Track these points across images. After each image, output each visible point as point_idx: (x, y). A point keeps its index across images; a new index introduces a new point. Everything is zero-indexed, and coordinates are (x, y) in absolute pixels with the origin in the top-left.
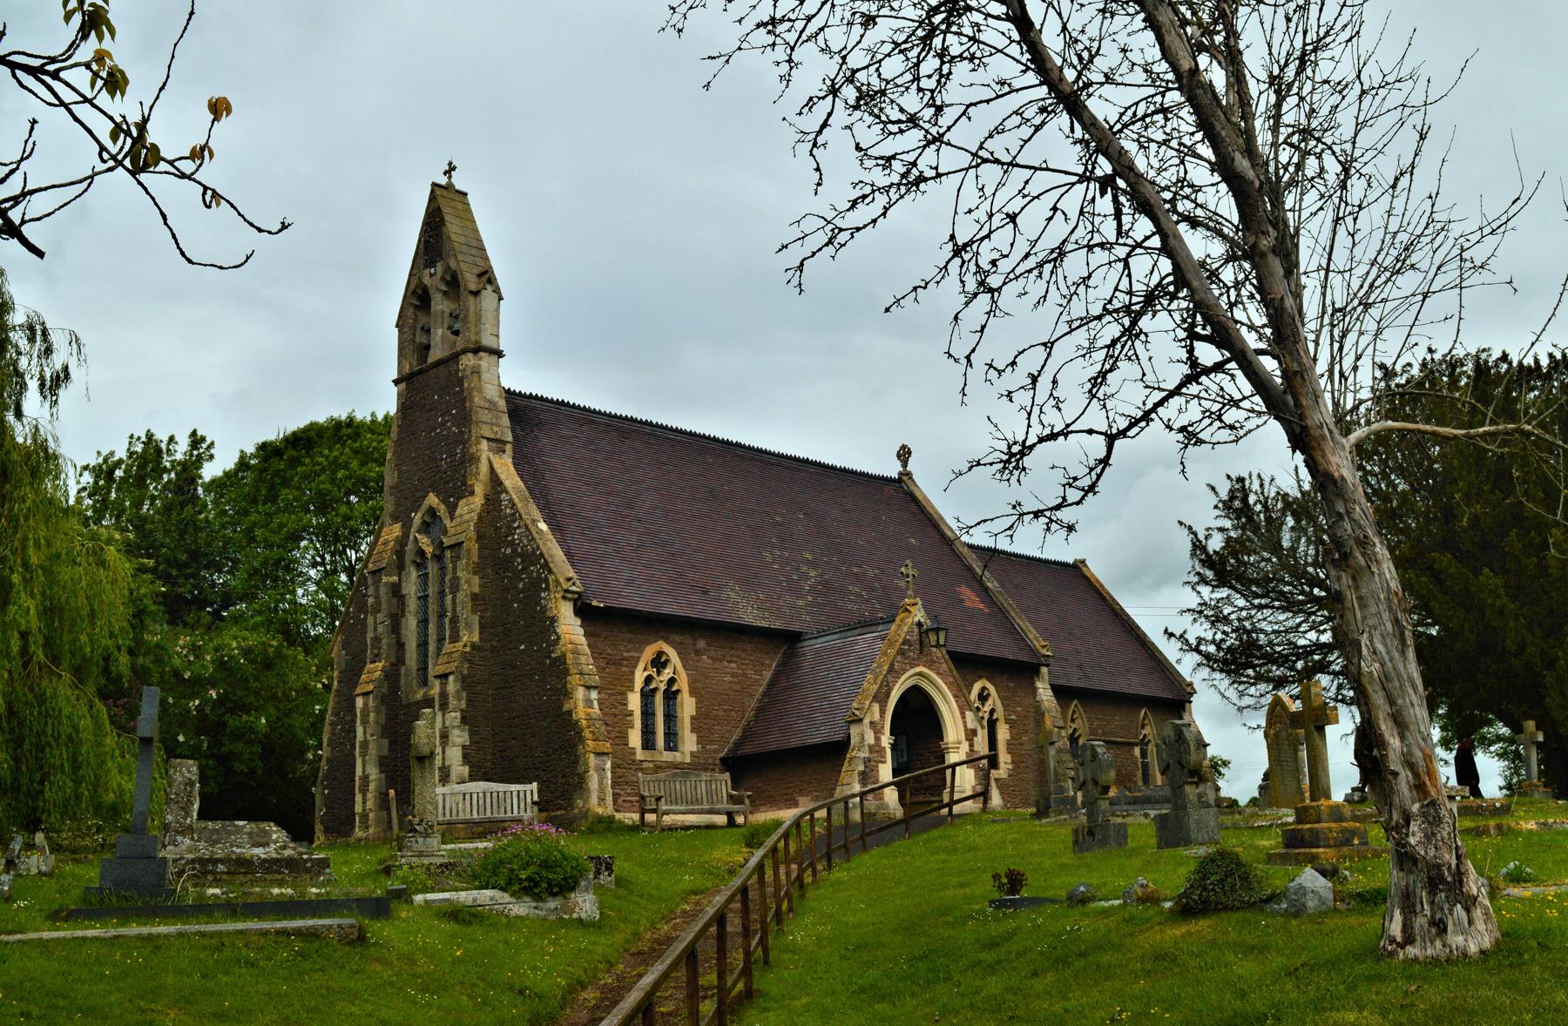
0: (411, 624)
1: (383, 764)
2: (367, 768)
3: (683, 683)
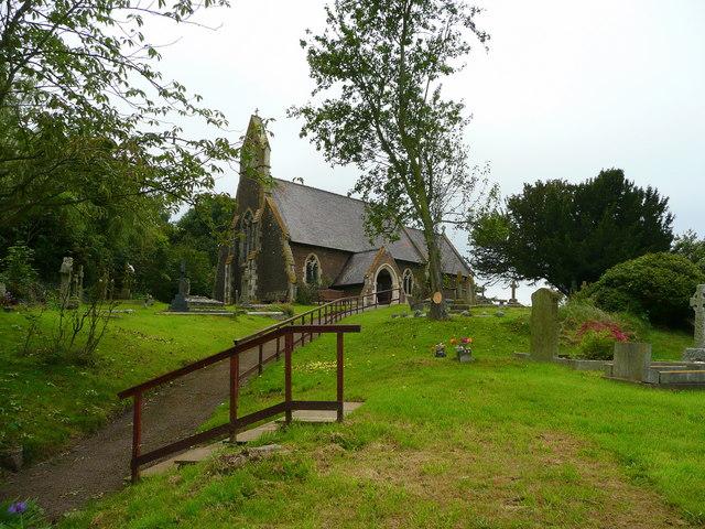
0: (241, 245)
1: (233, 284)
2: (228, 285)
3: (319, 264)
